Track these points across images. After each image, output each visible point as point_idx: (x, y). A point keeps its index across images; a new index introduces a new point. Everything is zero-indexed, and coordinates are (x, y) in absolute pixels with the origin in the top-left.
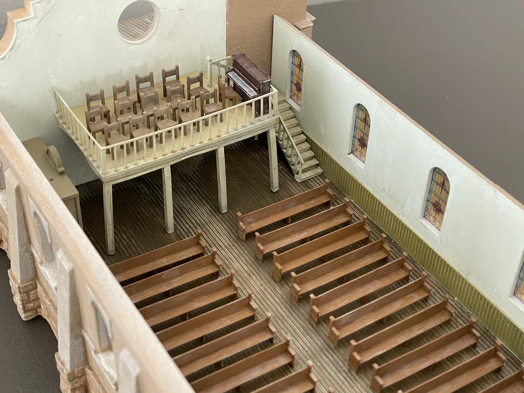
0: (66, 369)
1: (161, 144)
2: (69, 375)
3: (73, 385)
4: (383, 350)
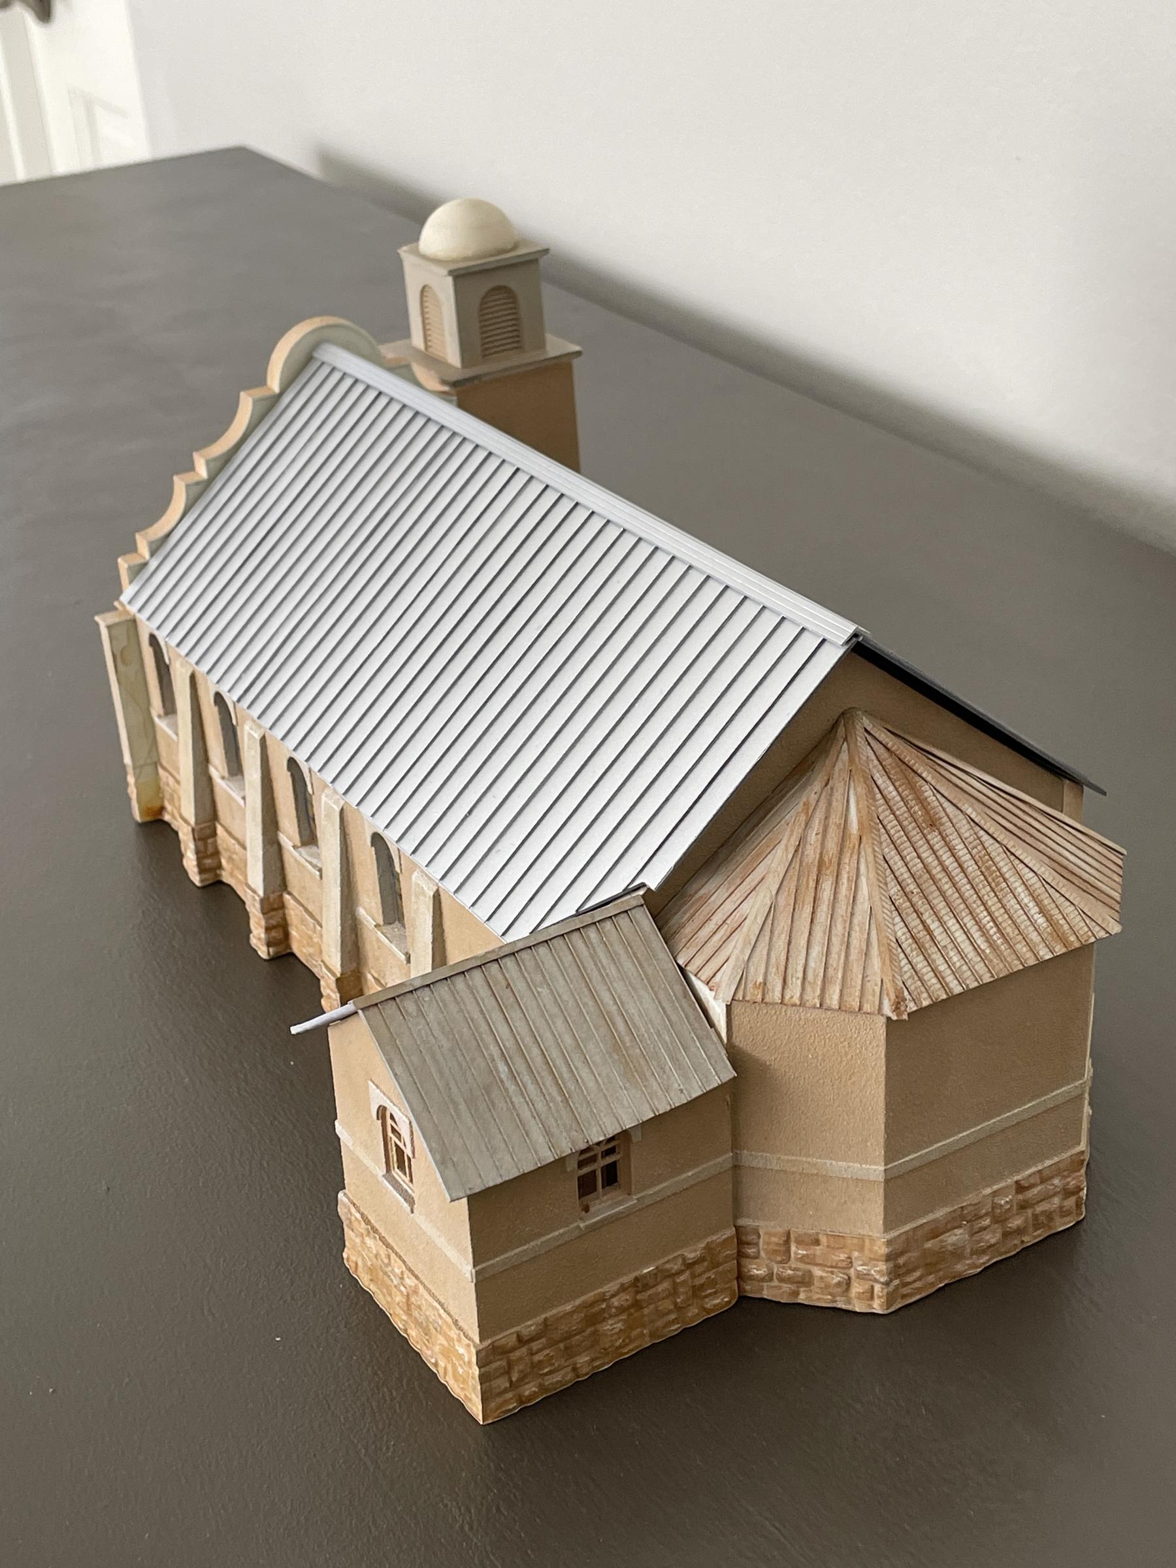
0: (258, 896)
1: (583, 1213)
2: (263, 901)
3: (267, 920)
4: (953, 1206)
